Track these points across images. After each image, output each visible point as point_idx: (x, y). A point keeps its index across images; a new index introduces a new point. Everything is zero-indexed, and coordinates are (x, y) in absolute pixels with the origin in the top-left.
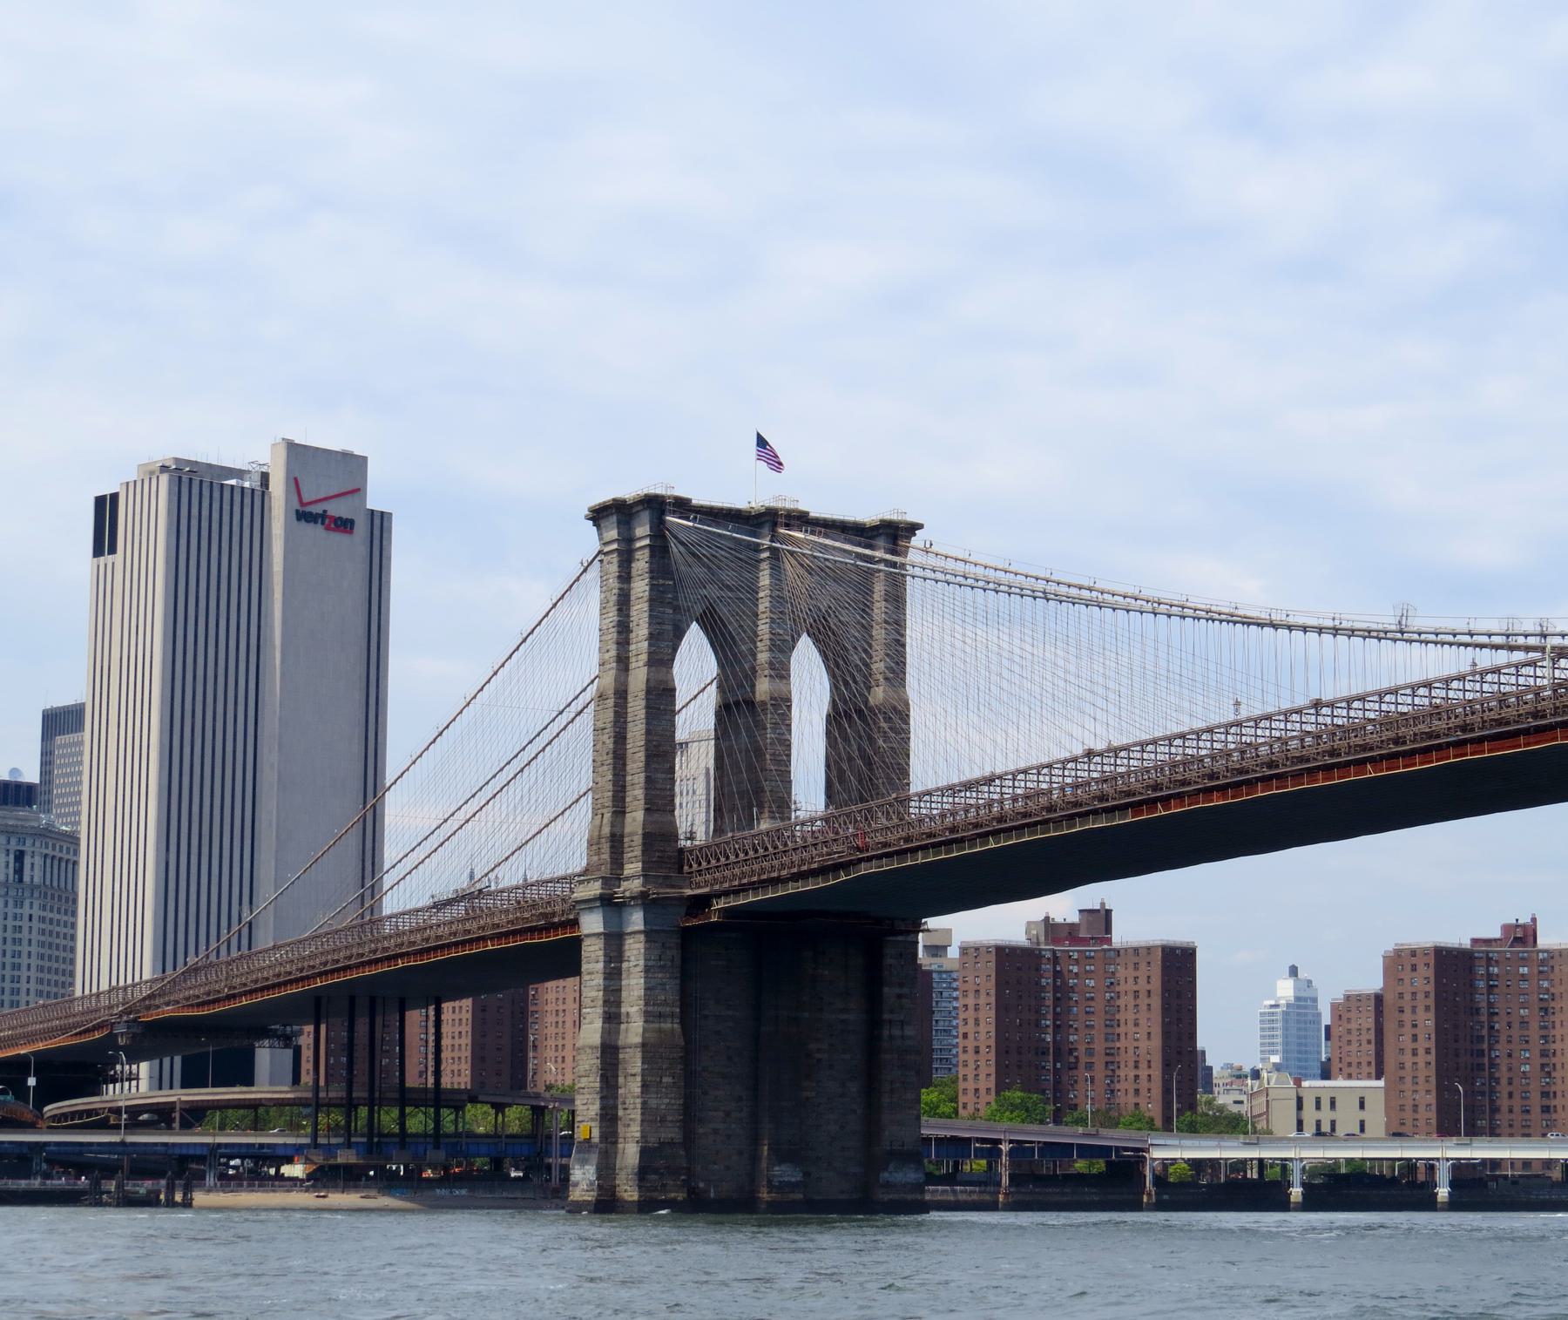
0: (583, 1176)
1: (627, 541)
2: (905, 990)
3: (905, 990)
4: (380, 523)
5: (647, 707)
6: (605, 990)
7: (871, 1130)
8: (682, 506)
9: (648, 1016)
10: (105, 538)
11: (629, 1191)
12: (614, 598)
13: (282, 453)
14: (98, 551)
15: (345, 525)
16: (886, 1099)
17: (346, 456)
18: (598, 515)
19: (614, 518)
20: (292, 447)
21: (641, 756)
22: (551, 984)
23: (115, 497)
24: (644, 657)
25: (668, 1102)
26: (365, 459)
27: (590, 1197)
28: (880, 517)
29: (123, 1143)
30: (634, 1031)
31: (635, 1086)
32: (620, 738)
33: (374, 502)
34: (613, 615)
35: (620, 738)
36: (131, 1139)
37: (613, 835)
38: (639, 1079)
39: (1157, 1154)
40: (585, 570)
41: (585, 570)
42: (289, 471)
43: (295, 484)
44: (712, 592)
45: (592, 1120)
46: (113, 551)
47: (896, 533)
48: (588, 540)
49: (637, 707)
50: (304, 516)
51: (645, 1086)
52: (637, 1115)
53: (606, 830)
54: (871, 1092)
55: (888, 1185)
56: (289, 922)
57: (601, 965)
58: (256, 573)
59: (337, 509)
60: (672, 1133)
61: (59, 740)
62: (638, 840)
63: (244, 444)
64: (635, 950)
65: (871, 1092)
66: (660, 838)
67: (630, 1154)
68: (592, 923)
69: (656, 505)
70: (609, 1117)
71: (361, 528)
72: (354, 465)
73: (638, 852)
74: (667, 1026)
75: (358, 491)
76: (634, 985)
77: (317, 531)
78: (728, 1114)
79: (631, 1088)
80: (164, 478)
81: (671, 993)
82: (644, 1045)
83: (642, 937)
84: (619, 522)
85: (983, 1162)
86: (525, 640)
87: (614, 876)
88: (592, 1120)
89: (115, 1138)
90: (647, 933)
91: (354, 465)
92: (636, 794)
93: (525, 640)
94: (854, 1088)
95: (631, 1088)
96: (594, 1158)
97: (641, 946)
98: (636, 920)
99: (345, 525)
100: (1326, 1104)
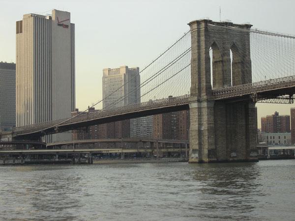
0: (194, 157)
1: (199, 29)
2: (253, 118)
3: (253, 118)
4: (73, 25)
7: (247, 146)
8: (210, 22)
9: (208, 124)
11: (206, 159)
13: (54, 12)
14: (17, 33)
15: (67, 26)
16: (250, 139)
17: (67, 12)
18: (190, 24)
20: (56, 11)
22: (131, 119)
23: (21, 21)
25: (212, 141)
26: (70, 13)
27: (197, 160)
28: (245, 23)
29: (74, 151)
30: (205, 127)
31: (206, 138)
32: (199, 68)
33: (72, 22)
34: (196, 44)
35: (199, 68)
36: (75, 150)
38: (207, 136)
39: (270, 148)
42: (56, 16)
43: (57, 18)
44: (215, 39)
45: (196, 145)
47: (248, 26)
48: (189, 28)
49: (203, 62)
50: (59, 25)
51: (208, 138)
52: (207, 144)
53: (197, 87)
54: (247, 138)
55: (251, 156)
57: (197, 114)
58: (51, 36)
60: (213, 147)
62: (205, 89)
63: (46, 11)
64: (205, 112)
65: (247, 138)
66: (208, 87)
67: (206, 151)
68: (194, 105)
69: (206, 22)
70: (200, 144)
71: (69, 27)
72: (68, 14)
73: (205, 91)
74: (212, 125)
75: (69, 20)
76: (205, 118)
77: (61, 28)
78: (222, 143)
80: (32, 17)
81: (212, 118)
82: (208, 130)
85: (197, 155)
87: (199, 95)
88: (196, 145)
89: (72, 150)
91: (68, 14)
92: (204, 79)
94: (244, 137)
96: (198, 152)
98: (205, 104)
99: (67, 26)
100: (272, 137)
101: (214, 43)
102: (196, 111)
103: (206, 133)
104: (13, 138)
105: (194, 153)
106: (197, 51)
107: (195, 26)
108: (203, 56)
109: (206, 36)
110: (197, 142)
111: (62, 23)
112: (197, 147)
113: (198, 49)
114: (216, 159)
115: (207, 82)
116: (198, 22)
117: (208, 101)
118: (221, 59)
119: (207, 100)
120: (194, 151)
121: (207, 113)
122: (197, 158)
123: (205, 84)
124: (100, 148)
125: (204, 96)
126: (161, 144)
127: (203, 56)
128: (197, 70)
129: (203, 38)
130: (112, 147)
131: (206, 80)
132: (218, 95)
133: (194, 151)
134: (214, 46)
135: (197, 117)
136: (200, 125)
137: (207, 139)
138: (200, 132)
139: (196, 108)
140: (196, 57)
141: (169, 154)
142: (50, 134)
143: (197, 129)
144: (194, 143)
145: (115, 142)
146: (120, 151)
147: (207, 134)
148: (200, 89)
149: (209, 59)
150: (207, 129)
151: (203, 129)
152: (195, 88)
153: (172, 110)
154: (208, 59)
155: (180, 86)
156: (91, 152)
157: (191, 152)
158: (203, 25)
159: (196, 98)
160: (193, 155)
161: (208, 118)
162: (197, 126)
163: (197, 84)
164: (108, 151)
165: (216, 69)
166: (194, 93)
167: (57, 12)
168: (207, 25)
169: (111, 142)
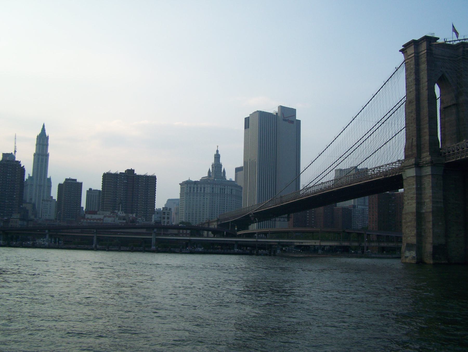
5: (428, 103)
6: (417, 194)
9: (433, 202)
10: (247, 125)
11: (429, 260)
12: (414, 71)
14: (245, 128)
19: (413, 46)
21: (427, 118)
24: (426, 88)
30: (428, 206)
31: (430, 225)
34: (413, 77)
37: (417, 144)
38: (431, 223)
40: (397, 70)
41: (397, 70)
45: (412, 236)
46: (248, 127)
48: (401, 57)
51: (433, 225)
52: (431, 235)
53: (415, 143)
56: (286, 196)
57: (415, 186)
59: (291, 119)
61: (238, 172)
64: (428, 183)
67: (429, 248)
70: (419, 235)
71: (295, 122)
72: (293, 111)
73: (427, 149)
75: (295, 115)
76: (428, 192)
79: (429, 225)
82: (433, 212)
83: (430, 176)
84: (414, 48)
85: (413, 253)
86: (374, 97)
87: (419, 156)
88: (412, 236)
90: (432, 175)
91: (293, 111)
93: (374, 97)
95: (429, 225)
97: (430, 180)
98: (428, 170)
99: (292, 122)
101: (443, 76)
102: (413, 181)
103: (430, 218)
104: (218, 225)
105: (409, 250)
106: (414, 88)
107: (411, 50)
108: (425, 93)
109: (429, 62)
110: (414, 233)
111: (287, 119)
112: (414, 240)
113: (416, 84)
114: (447, 262)
115: (430, 135)
116: (415, 43)
117: (432, 164)
118: (454, 102)
119: (432, 162)
120: (410, 247)
121: (431, 185)
122: (414, 257)
123: (427, 138)
124: (292, 239)
125: (426, 157)
126: (371, 236)
127: (425, 93)
128: (414, 116)
129: (424, 66)
130: (306, 238)
131: (430, 131)
132: (449, 155)
133: (410, 247)
134: (442, 82)
135: (414, 191)
136: (420, 203)
137: (431, 227)
138: (419, 216)
139: (413, 177)
140: (413, 96)
141: (383, 249)
142: (263, 221)
143: (414, 210)
144: (409, 234)
145: (313, 232)
146: (318, 244)
147: (431, 218)
148: (419, 147)
149: (435, 99)
150: (431, 210)
151: (424, 211)
152: (412, 146)
153: (381, 185)
154: (432, 97)
155: (387, 149)
156: (279, 242)
157: (403, 248)
158: (424, 45)
159: (413, 161)
160: (407, 254)
161: (433, 193)
162: (414, 205)
163: (415, 139)
164: (302, 243)
165: (446, 119)
166: (410, 153)
167: (282, 108)
168: (430, 45)
169: (308, 232)
